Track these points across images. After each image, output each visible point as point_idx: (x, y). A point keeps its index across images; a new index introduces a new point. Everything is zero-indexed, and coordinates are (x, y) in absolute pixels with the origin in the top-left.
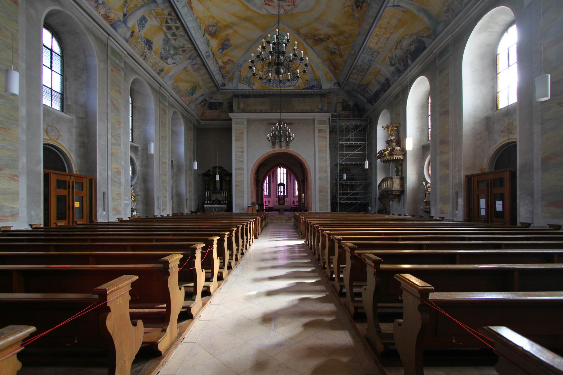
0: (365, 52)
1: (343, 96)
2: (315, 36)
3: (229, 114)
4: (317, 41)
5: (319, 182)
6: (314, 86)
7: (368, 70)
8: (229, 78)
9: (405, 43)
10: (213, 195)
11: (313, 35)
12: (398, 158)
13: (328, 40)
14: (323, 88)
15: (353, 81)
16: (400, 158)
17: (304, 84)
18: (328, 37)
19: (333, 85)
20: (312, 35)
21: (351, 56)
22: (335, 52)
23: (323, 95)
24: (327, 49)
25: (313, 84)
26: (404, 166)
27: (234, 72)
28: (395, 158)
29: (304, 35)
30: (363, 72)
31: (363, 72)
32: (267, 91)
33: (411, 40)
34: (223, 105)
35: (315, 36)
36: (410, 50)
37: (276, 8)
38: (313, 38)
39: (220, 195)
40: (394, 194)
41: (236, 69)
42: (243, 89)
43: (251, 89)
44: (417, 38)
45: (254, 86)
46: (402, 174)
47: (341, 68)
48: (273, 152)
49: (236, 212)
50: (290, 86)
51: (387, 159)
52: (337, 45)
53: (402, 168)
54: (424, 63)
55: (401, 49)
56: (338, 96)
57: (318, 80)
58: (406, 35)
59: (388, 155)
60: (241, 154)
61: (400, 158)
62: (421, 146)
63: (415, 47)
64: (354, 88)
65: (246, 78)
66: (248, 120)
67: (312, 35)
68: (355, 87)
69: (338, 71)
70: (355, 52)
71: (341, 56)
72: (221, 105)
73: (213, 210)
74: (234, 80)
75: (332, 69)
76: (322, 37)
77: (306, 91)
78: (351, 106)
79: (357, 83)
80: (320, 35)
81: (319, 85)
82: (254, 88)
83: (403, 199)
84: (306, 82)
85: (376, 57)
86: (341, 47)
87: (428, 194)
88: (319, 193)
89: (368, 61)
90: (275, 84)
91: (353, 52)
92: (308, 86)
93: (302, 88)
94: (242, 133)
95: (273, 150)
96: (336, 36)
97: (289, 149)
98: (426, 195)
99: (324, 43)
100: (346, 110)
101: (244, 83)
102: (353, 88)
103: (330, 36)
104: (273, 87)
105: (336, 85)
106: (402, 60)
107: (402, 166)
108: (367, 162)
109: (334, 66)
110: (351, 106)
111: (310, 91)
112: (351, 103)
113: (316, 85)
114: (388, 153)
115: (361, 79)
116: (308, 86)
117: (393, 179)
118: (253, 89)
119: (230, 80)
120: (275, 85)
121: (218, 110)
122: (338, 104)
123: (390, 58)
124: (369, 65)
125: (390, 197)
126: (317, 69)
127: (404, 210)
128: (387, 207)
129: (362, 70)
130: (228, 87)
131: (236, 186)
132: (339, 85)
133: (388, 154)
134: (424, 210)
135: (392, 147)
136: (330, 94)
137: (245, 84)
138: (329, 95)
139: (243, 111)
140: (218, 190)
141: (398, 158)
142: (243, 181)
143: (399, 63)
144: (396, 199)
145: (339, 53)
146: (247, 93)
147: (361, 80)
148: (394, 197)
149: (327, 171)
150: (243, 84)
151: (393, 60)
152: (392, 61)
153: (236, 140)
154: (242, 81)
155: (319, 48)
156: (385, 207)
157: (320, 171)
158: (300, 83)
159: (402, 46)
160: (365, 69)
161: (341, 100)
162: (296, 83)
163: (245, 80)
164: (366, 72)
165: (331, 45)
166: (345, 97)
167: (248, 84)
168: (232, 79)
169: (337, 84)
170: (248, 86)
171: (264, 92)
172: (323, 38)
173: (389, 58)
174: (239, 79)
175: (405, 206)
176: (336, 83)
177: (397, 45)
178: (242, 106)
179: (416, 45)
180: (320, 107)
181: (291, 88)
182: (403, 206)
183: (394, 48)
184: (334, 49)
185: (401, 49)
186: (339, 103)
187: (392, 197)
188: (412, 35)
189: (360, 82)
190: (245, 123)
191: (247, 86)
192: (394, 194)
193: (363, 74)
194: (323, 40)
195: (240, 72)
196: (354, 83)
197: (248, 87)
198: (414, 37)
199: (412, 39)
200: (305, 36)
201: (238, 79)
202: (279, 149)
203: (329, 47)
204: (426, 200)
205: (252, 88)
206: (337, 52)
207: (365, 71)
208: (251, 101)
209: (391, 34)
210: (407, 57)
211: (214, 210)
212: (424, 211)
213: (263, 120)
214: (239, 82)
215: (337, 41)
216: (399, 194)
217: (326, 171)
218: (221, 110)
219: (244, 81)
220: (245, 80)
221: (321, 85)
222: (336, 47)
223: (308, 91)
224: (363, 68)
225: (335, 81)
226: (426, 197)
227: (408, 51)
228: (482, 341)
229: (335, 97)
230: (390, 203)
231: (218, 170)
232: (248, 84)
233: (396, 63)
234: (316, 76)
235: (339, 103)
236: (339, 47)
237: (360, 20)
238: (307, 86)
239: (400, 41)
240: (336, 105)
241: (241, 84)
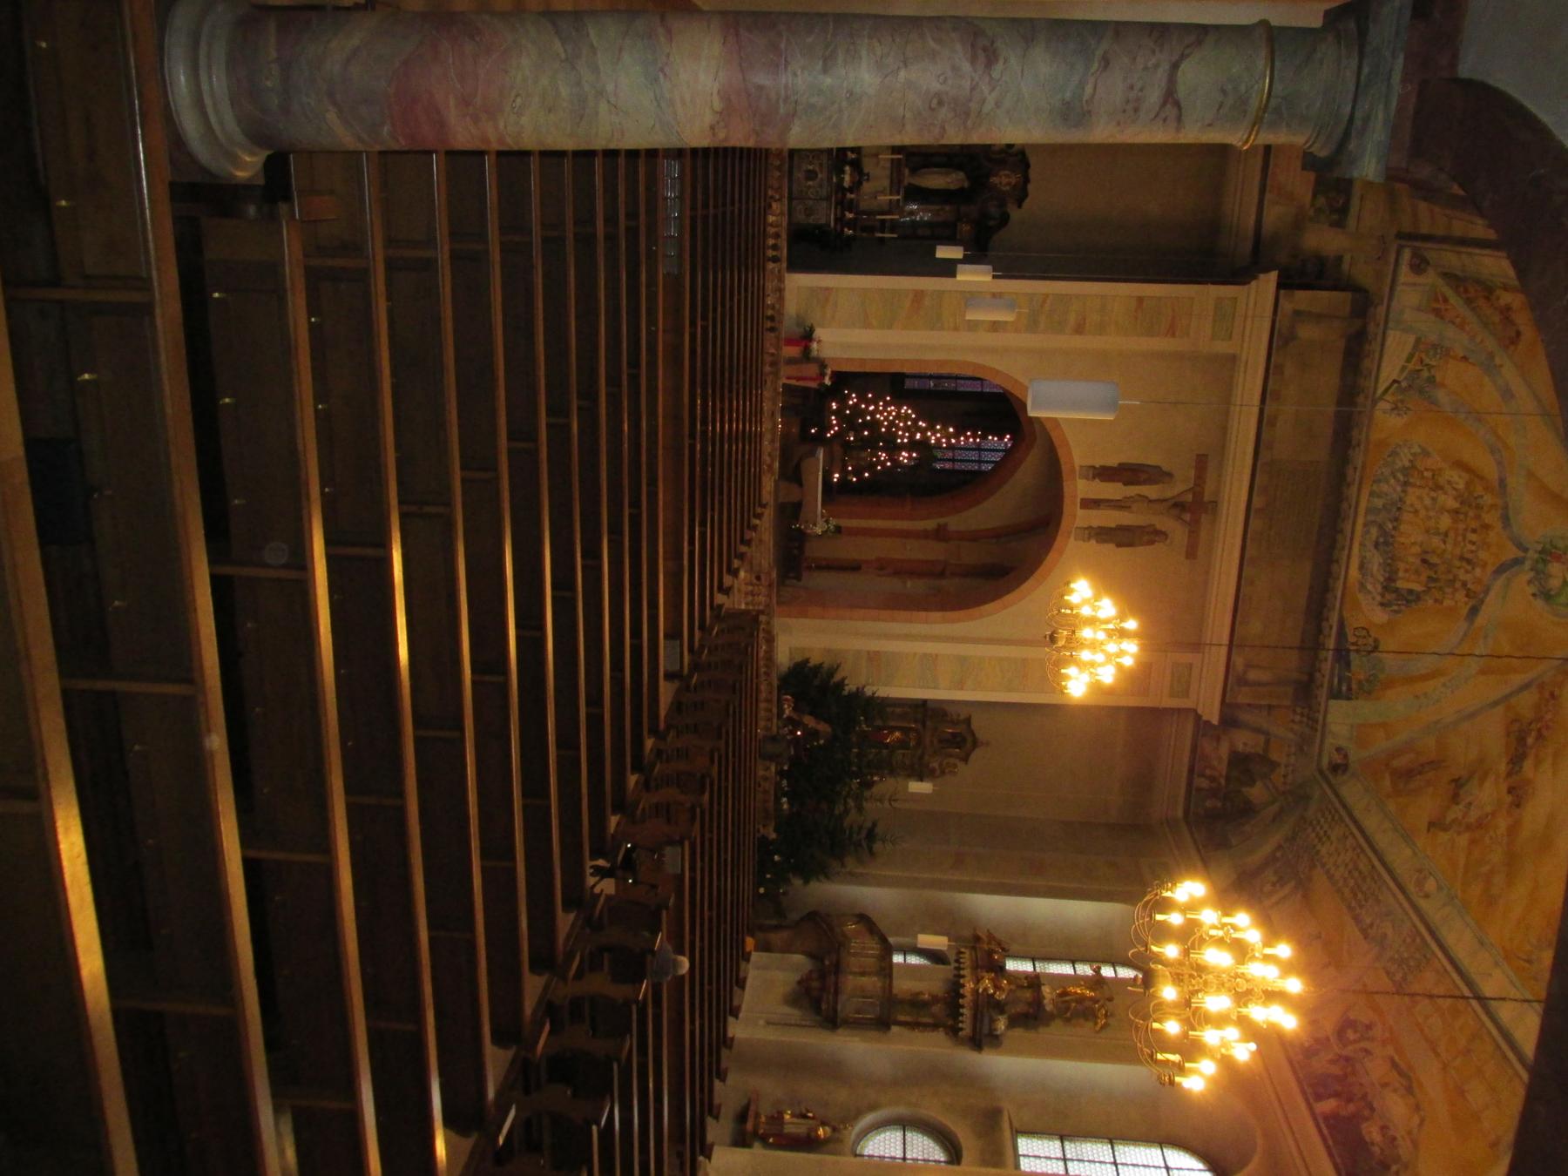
0: (1414, 941)
1: (1291, 768)
2: (1540, 736)
3: (1274, 275)
4: (1521, 740)
5: (915, 654)
6: (1348, 664)
7: (1357, 919)
8: (1446, 300)
9: (1396, 1107)
10: (888, 165)
11: (1545, 733)
13: (1510, 791)
14: (1332, 702)
15: (1333, 838)
16: (961, 1029)
17: (1363, 628)
18: (1518, 794)
19: (1342, 743)
20: (1548, 727)
21: (1420, 871)
22: (1457, 804)
23: (1305, 691)
24: (1479, 770)
25: (1353, 668)
27: (1467, 328)
28: (962, 1015)
29: (1557, 692)
30: (1355, 895)
31: (1355, 895)
32: (1358, 457)
33: (1398, 1136)
34: (1332, 225)
35: (1540, 736)
36: (1367, 1119)
38: (1533, 726)
39: (886, 183)
41: (1482, 341)
42: (1386, 358)
43: (1380, 391)
44: (1397, 1159)
45: (1388, 406)
47: (1391, 806)
48: (1065, 468)
49: (788, 295)
50: (1362, 567)
52: (1480, 825)
54: (1298, 1161)
55: (1385, 1085)
56: (1293, 749)
57: (1370, 688)
58: (1422, 1121)
59: (978, 990)
60: (1072, 319)
61: (961, 1029)
63: (1373, 1144)
64: (1310, 830)
65: (1431, 380)
66: (1233, 359)
67: (1548, 727)
68: (1313, 835)
69: (1387, 782)
70: (1427, 896)
71: (1435, 825)
72: (1335, 217)
73: (811, 167)
74: (1432, 317)
75: (1399, 763)
76: (1528, 764)
77: (1331, 627)
78: (1244, 790)
79: (1324, 851)
80: (1538, 762)
81: (1349, 689)
82: (1382, 405)
84: (1371, 641)
85: (1388, 973)
86: (1463, 840)
88: (868, 652)
89: (1385, 935)
90: (1384, 506)
91: (1430, 885)
92: (1353, 644)
93: (1345, 614)
94: (1171, 331)
95: (1077, 468)
96: (1513, 830)
97: (1072, 539)
99: (1503, 767)
101: (1411, 366)
102: (1311, 824)
103: (1518, 806)
104: (1372, 494)
105: (1338, 759)
106: (1346, 1076)
107: (934, 1026)
109: (1409, 774)
110: (1244, 790)
111: (1331, 643)
112: (1256, 792)
113: (1349, 679)
114: (986, 989)
115: (1333, 875)
116: (1353, 644)
118: (1375, 402)
119: (1436, 300)
120: (1379, 503)
121: (1314, 196)
122: (1262, 739)
123: (1369, 1027)
124: (1369, 931)
126: (1417, 697)
129: (1360, 895)
130: (1403, 284)
131: (919, 296)
132: (1335, 768)
133: (981, 990)
134: (752, 1108)
136: (1305, 719)
137: (1403, 368)
138: (1302, 715)
139: (1280, 339)
140: (909, 179)
141: (962, 1022)
142: (942, 329)
143: (1340, 1056)
145: (1448, 820)
146: (1366, 363)
147: (1331, 877)
149: (962, 689)
150: (1408, 360)
151: (1358, 1035)
152: (1356, 1032)
153: (1140, 300)
154: (1423, 356)
155: (1491, 737)
157: (962, 660)
158: (1369, 612)
159: (1395, 1091)
160: (1361, 907)
161: (1274, 756)
162: (1374, 599)
163: (1425, 374)
164: (1350, 908)
165: (1487, 795)
166: (1285, 776)
167: (1404, 384)
168: (1437, 313)
169: (1339, 761)
170: (1395, 381)
171: (1359, 445)
172: (1521, 767)
173: (1367, 1022)
174: (1435, 347)
176: (1346, 756)
177: (1401, 1073)
178: (1307, 332)
179: (1376, 1150)
180: (1253, 675)
181: (1354, 572)
183: (1396, 1058)
184: (1470, 804)
185: (1385, 1085)
186: (1267, 742)
188: (1415, 1144)
189: (1323, 865)
190: (1221, 347)
191: (1394, 376)
193: (1347, 891)
194: (1517, 768)
195: (1465, 358)
196: (1324, 839)
197: (1390, 381)
198: (1404, 1149)
199: (1403, 1137)
200: (1552, 695)
201: (1433, 338)
202: (1080, 495)
203: (1482, 780)
204: (787, 1117)
205: (1381, 398)
206: (1456, 812)
207: (1353, 904)
208: (1328, 379)
209: (1445, 1067)
210: (1350, 1100)
211: (809, 171)
213: (1224, 430)
214: (1418, 341)
215: (1492, 833)
217: (960, 685)
218: (1311, 213)
219: (1420, 368)
220: (1425, 374)
221: (1349, 699)
222: (1474, 815)
223: (1330, 636)
224: (1366, 901)
225: (1355, 755)
227: (1366, 1113)
228: (549, 440)
229: (1291, 736)
231: (1009, 184)
232: (1404, 384)
233: (1345, 1046)
234: (1390, 684)
235: (1267, 742)
236: (1469, 828)
237: (1527, 965)
238: (1351, 639)
239: (1409, 1090)
240: (1258, 730)
241: (1409, 348)
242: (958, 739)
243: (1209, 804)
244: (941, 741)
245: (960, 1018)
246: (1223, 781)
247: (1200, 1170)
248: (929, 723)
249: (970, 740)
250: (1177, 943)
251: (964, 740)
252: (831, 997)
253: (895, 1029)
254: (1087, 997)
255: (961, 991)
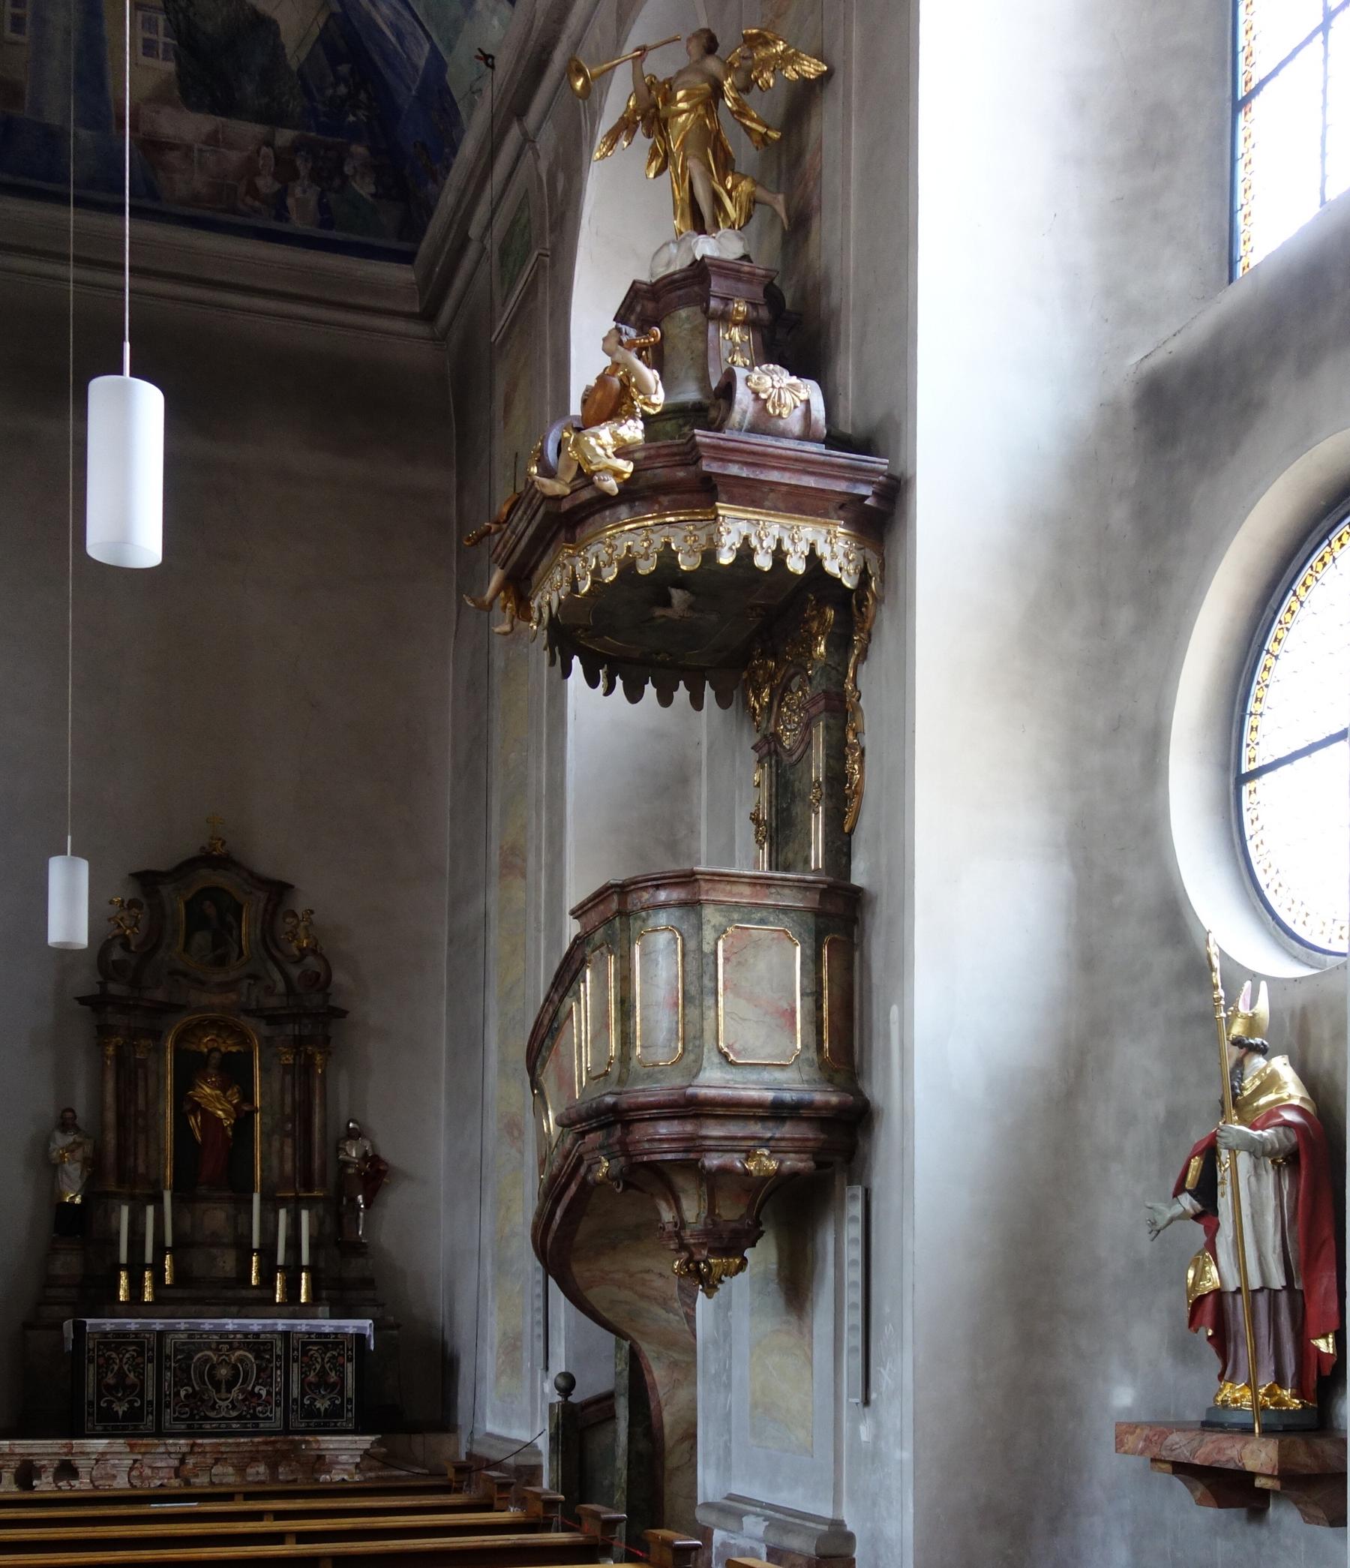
12: (779, 556)
16: (813, 560)
26: (871, 729)
28: (746, 553)
37: (854, 1219)
40: (713, 1161)
46: (840, 848)
51: (610, 575)
53: (839, 752)
61: (813, 560)
62: (1127, 393)
83: (853, 1253)
87: (1244, 1160)
98: (1206, 1191)
100: (224, 105)
108: (125, 405)
110: (294, 66)
114: (623, 451)
117: (711, 916)
125: (667, 1216)
127: (865, 1433)
128: (658, 1373)
133: (627, 467)
134: (1184, 1446)
135: (704, 379)
141: (779, 556)
144: (762, 1256)
148: (730, 1212)
156: (635, 1359)
175: (883, 1377)
182: (852, 1364)
187: (692, 1209)
192: (724, 1171)
212: (1181, 1468)
216: (792, 1162)
226: (1207, 1213)
230: (691, 1319)
242: (209, 909)
243: (365, 188)
244: (221, 961)
245: (763, 561)
246: (285, 136)
247: (1325, 42)
248: (159, 995)
249: (208, 877)
250: (770, 312)
251: (213, 893)
252: (715, 1130)
253: (859, 876)
254: (699, 121)
255: (646, 567)
